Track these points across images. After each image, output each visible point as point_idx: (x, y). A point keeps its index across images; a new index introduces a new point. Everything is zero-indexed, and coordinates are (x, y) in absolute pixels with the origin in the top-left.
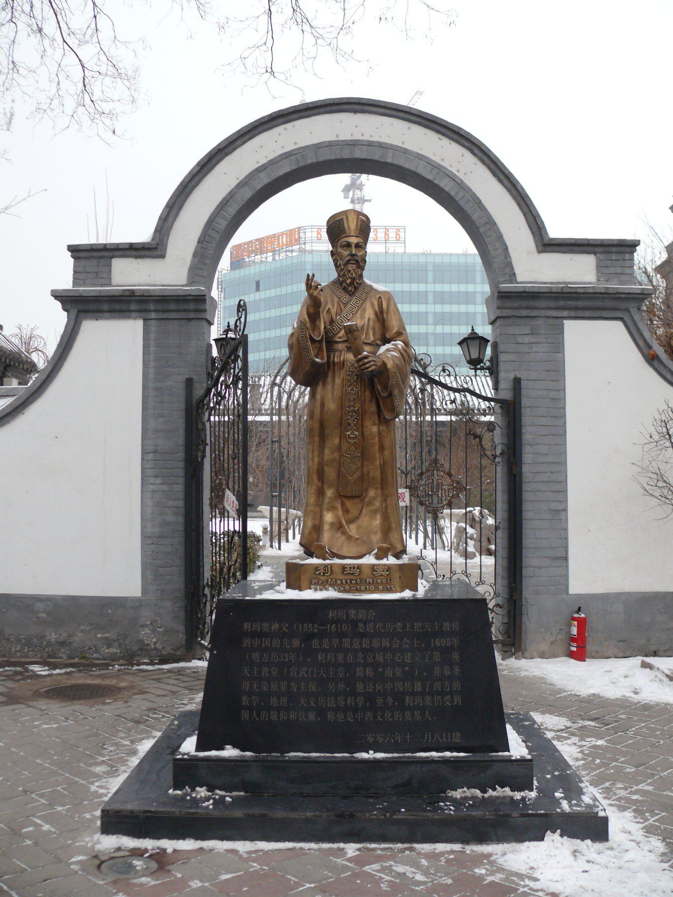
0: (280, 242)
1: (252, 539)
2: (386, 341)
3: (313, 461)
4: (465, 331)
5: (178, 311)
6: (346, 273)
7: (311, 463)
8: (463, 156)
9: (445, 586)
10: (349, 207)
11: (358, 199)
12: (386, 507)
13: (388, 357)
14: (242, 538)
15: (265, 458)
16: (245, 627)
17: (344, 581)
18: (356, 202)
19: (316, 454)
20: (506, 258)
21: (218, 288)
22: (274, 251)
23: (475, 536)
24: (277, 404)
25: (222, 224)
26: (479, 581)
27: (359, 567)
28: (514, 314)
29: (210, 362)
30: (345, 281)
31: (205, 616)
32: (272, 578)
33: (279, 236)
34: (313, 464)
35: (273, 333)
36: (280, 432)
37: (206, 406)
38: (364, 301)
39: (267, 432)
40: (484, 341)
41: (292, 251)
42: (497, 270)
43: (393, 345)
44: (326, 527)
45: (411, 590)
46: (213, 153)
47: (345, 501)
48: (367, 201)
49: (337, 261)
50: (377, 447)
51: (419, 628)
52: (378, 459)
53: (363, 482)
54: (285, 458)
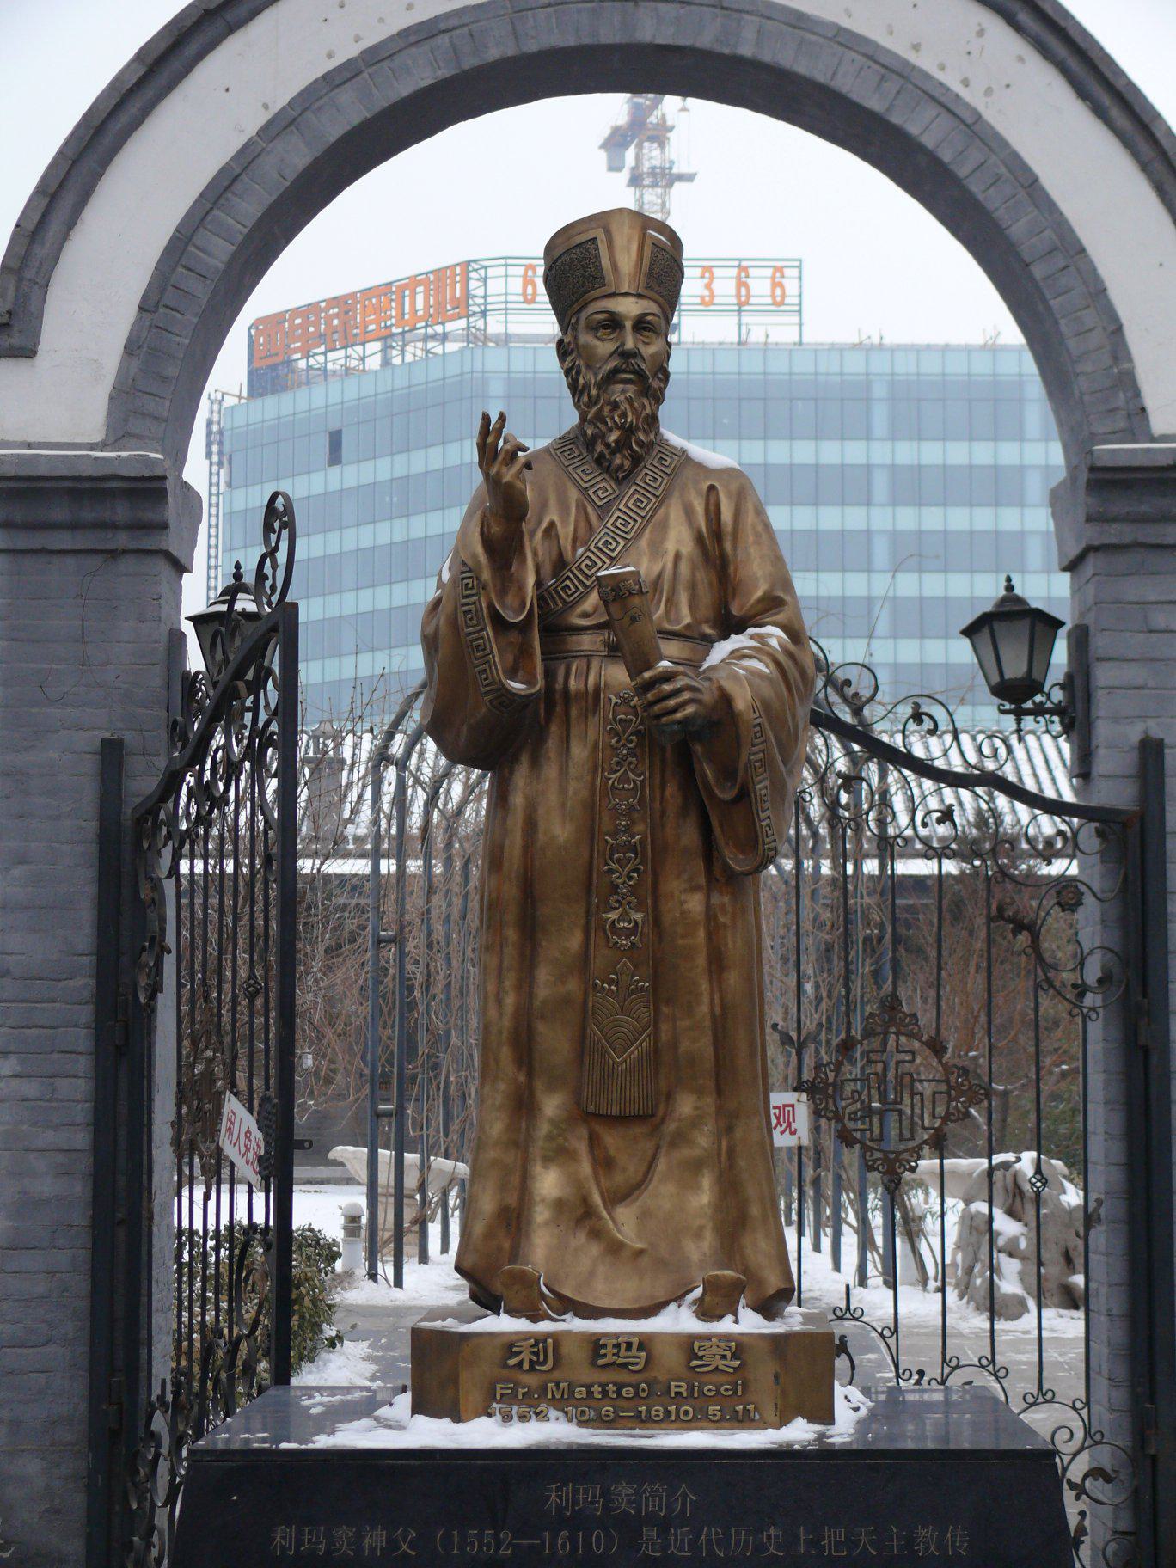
0: (407, 309)
1: (310, 1251)
2: (730, 625)
3: (499, 1002)
4: (987, 591)
5: (74, 526)
6: (607, 409)
7: (493, 1013)
8: (981, 33)
9: (930, 1407)
10: (625, 199)
11: (653, 172)
12: (731, 1152)
13: (735, 677)
14: (273, 1251)
15: (356, 992)
16: (278, 1539)
17: (596, 1389)
18: (647, 181)
19: (510, 981)
20: (1116, 359)
21: (209, 454)
22: (386, 338)
23: (1023, 1244)
24: (394, 822)
25: (218, 251)
26: (1035, 1391)
27: (645, 1342)
28: (1141, 539)
29: (177, 687)
30: (603, 436)
31: (153, 1505)
32: (373, 1379)
33: (402, 289)
34: (501, 1015)
35: (383, 598)
36: (401, 911)
37: (165, 830)
38: (662, 500)
39: (361, 910)
40: (1045, 624)
41: (444, 338)
42: (1086, 398)
43: (752, 637)
44: (541, 1214)
45: (812, 1419)
46: (189, 23)
47: (598, 1128)
48: (681, 178)
49: (578, 372)
50: (701, 960)
51: (838, 1543)
52: (706, 999)
53: (657, 1072)
54: (417, 993)
